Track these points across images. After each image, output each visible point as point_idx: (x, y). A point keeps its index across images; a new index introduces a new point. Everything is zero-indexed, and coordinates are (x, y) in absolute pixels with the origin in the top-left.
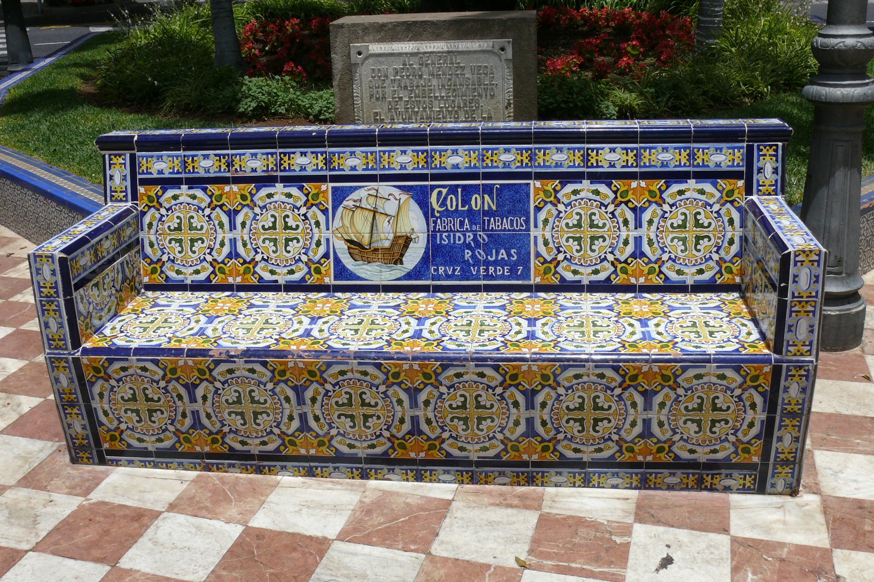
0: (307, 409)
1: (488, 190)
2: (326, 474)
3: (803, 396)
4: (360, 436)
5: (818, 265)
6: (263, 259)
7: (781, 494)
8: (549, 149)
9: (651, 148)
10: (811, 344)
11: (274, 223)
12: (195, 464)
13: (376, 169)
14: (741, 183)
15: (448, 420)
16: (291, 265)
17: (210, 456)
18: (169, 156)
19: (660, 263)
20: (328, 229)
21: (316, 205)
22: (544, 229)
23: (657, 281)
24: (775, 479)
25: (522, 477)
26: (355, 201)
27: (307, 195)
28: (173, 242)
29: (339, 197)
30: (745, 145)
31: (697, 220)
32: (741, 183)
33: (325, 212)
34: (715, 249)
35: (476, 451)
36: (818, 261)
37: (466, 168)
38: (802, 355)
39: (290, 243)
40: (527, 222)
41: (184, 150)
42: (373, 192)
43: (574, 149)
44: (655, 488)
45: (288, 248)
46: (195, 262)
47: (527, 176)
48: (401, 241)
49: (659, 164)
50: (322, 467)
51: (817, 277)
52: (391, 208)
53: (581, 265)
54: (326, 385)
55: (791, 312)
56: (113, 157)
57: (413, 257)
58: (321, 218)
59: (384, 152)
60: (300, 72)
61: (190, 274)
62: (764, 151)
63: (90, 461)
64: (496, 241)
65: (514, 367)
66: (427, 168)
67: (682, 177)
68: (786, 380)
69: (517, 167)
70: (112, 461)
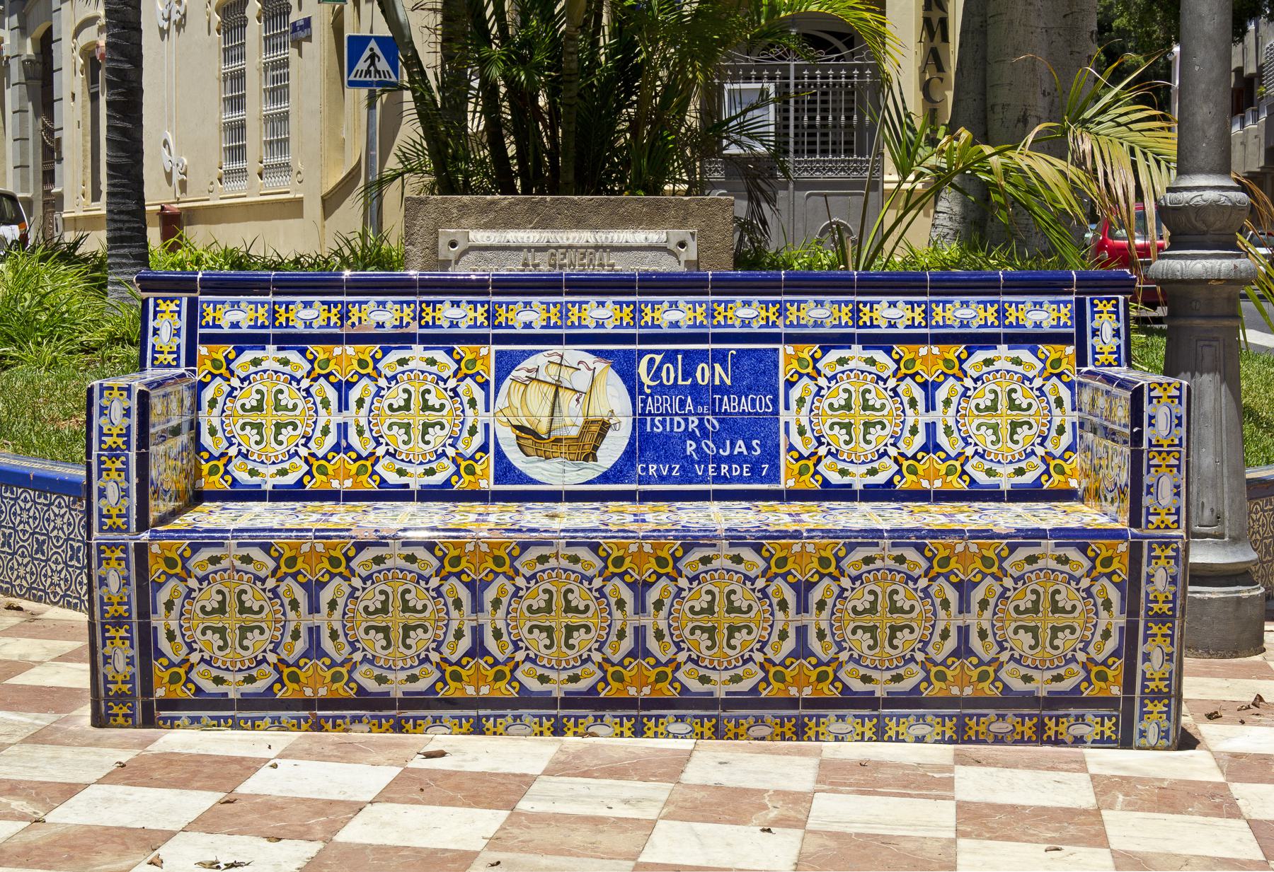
0: (484, 619)
1: (720, 357)
2: (500, 729)
3: (1173, 589)
4: (559, 662)
5: (1180, 403)
6: (388, 453)
7: (1154, 748)
8: (806, 302)
9: (945, 303)
10: (1178, 512)
11: (408, 401)
12: (298, 719)
13: (561, 327)
14: (1070, 350)
15: (687, 632)
16: (430, 461)
17: (326, 704)
18: (250, 303)
19: (962, 459)
20: (487, 410)
21: (472, 376)
22: (798, 412)
23: (959, 485)
24: (1144, 723)
25: (788, 725)
26: (529, 371)
27: (458, 362)
28: (248, 428)
29: (505, 365)
30: (1073, 298)
31: (1011, 400)
32: (1070, 350)
33: (484, 386)
34: (1039, 440)
35: (724, 683)
36: (1179, 397)
37: (689, 327)
38: (1167, 527)
39: (430, 430)
40: (775, 401)
41: (275, 294)
42: (556, 359)
43: (839, 303)
44: (978, 742)
45: (427, 438)
46: (281, 457)
47: (775, 338)
48: (595, 428)
49: (957, 324)
50: (496, 717)
51: (1179, 418)
52: (581, 380)
53: (852, 462)
54: (517, 579)
55: (1149, 466)
56: (160, 301)
57: (612, 450)
58: (479, 395)
59: (574, 304)
60: (482, 161)
61: (272, 476)
62: (1100, 307)
63: (130, 721)
64: (732, 427)
65: (783, 547)
66: (634, 326)
67: (989, 341)
68: (1149, 564)
69: (761, 327)
70: (165, 719)
